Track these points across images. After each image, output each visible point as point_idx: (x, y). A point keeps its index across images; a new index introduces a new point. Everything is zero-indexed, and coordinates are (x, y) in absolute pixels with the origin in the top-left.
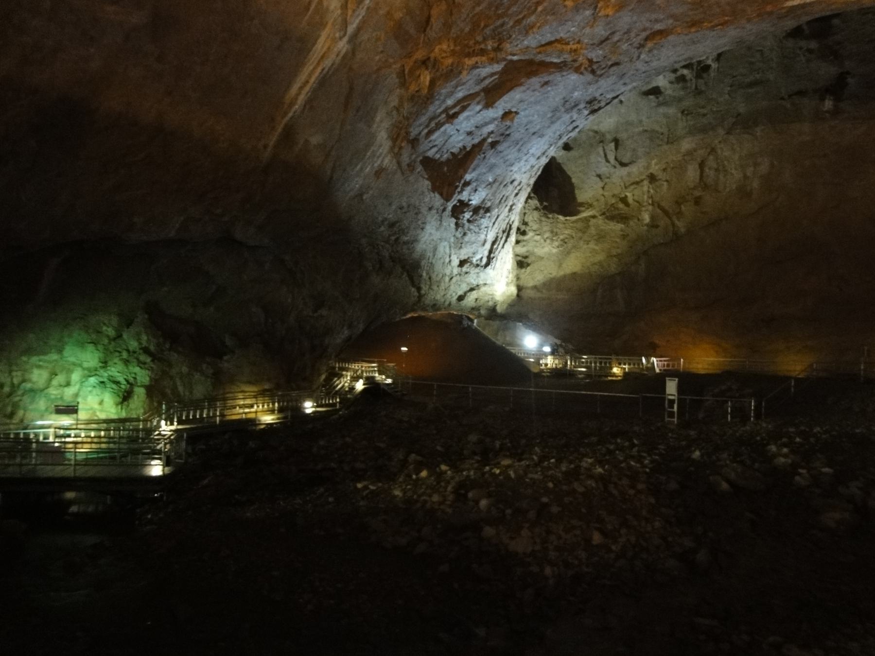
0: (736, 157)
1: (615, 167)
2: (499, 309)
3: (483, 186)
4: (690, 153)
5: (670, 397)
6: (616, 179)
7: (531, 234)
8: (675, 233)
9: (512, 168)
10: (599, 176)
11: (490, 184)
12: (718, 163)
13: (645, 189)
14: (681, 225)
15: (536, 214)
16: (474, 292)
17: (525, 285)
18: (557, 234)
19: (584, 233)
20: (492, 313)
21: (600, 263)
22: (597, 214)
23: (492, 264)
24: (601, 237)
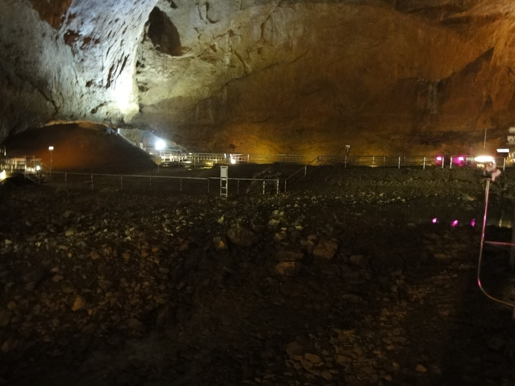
0: (284, 23)
1: (207, 23)
2: (126, 120)
3: (90, 20)
4: (255, 17)
5: (223, 179)
6: (207, 32)
7: (147, 67)
8: (246, 72)
9: (113, 8)
10: (196, 29)
11: (94, 19)
12: (272, 27)
13: (227, 40)
14: (249, 67)
15: (151, 53)
16: (104, 107)
17: (146, 104)
18: (166, 68)
19: (186, 68)
20: (121, 123)
21: (197, 90)
22: (195, 56)
23: (113, 85)
24: (198, 72)
